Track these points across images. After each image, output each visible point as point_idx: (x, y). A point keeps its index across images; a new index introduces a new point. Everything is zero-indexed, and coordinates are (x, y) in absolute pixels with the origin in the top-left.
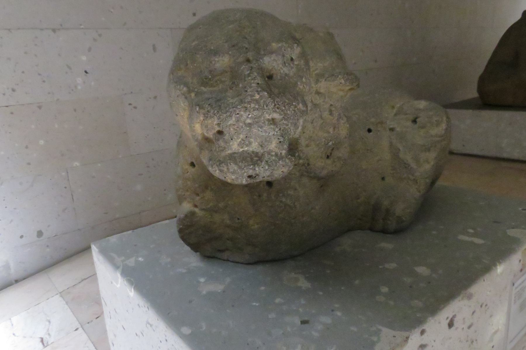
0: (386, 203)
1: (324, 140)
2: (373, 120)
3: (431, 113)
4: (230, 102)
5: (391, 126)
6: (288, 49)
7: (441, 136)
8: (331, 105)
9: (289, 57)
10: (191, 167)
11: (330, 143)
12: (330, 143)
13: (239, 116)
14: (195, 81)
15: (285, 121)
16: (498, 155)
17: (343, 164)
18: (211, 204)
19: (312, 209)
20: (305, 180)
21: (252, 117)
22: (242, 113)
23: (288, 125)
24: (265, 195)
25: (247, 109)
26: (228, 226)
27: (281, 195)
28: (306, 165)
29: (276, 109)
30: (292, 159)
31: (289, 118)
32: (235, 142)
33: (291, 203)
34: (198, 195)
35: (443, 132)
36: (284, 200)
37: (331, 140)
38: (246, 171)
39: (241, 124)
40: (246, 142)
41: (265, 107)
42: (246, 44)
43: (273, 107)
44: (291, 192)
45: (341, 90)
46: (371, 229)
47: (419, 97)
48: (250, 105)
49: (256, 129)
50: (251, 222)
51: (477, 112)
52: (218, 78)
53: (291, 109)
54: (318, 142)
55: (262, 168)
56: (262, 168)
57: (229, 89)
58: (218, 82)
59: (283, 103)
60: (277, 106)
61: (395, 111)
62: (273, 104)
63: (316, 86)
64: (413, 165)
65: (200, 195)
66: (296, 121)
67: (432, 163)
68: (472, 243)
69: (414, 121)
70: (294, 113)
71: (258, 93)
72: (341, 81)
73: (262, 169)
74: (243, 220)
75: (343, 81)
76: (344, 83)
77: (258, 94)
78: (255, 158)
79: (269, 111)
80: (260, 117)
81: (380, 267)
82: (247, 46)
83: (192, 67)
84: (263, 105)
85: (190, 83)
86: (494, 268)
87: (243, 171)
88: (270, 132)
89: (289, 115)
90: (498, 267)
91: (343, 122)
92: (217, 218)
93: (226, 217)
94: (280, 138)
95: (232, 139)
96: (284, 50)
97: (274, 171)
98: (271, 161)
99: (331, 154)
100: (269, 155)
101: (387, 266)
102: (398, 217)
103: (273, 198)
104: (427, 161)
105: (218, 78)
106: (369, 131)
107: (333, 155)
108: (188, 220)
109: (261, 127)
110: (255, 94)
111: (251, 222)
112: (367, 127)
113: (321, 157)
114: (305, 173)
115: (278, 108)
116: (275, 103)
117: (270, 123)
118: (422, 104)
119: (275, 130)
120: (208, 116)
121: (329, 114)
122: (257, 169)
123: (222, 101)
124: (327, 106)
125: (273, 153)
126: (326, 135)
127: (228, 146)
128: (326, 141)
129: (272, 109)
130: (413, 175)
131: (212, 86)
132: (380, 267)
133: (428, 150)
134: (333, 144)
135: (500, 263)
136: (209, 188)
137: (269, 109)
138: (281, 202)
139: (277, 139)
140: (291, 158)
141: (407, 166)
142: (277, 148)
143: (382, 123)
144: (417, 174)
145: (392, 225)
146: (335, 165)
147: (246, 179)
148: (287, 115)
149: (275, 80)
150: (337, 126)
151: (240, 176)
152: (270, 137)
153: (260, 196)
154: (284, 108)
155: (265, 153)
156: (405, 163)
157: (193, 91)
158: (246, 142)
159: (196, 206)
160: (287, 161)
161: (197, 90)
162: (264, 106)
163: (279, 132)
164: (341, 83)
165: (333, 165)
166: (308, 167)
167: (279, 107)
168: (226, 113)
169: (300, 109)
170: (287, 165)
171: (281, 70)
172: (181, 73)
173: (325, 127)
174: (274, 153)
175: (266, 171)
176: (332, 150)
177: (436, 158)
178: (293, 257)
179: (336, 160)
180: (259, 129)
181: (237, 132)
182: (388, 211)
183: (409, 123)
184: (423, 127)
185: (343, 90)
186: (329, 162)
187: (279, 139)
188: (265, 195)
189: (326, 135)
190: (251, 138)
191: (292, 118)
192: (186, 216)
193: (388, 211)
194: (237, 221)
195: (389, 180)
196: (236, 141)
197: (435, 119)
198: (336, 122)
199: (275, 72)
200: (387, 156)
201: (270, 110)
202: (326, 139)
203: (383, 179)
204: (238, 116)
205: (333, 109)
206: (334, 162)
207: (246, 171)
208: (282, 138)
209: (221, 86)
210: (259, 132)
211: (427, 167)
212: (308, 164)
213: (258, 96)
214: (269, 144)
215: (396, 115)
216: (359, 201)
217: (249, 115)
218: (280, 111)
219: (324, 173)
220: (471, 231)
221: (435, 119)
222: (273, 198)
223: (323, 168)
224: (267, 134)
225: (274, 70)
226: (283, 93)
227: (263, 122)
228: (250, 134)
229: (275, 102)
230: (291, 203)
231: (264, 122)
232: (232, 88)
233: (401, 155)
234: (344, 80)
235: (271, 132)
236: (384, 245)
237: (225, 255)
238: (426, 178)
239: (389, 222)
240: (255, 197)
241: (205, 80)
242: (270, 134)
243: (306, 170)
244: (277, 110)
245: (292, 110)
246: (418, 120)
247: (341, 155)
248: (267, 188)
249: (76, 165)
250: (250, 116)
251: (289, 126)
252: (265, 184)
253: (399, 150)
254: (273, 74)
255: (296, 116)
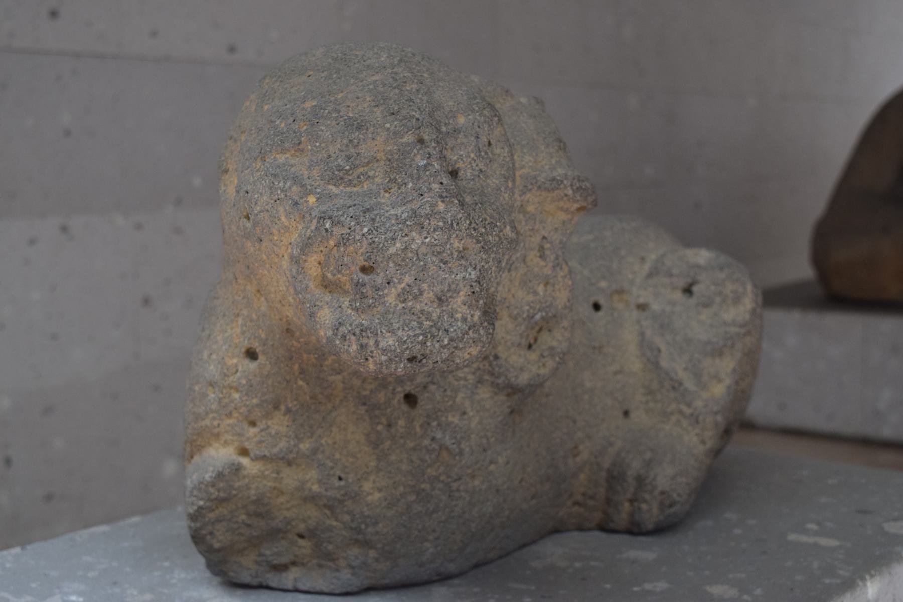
0: (635, 466)
1: (527, 308)
2: (603, 284)
3: (722, 276)
4: (390, 214)
5: (641, 300)
6: (485, 126)
7: (742, 326)
8: (544, 238)
9: (485, 140)
10: (247, 361)
11: (538, 316)
12: (538, 316)
13: (408, 240)
14: (315, 173)
15: (484, 254)
16: (870, 430)
17: (559, 363)
18: (283, 445)
19: (491, 462)
20: (484, 393)
21: (430, 242)
22: (414, 234)
23: (487, 263)
24: (401, 423)
25: (423, 228)
26: (311, 499)
27: (435, 424)
28: (491, 358)
29: (472, 230)
30: (489, 329)
31: (490, 248)
32: (393, 290)
33: (453, 444)
34: (253, 424)
35: (748, 316)
36: (439, 435)
37: (539, 310)
38: (410, 347)
39: (410, 255)
40: (413, 291)
41: (454, 225)
42: (416, 112)
43: (467, 226)
44: (454, 419)
45: (562, 209)
46: (604, 528)
47: (689, 243)
48: (430, 220)
49: (436, 266)
50: (367, 486)
51: (813, 318)
52: (361, 170)
53: (494, 233)
54: (515, 312)
55: (438, 341)
56: (438, 341)
57: (382, 191)
58: (362, 177)
59: (482, 221)
60: (473, 225)
61: (647, 267)
62: (468, 222)
63: (522, 198)
64: (689, 384)
65: (258, 424)
66: (501, 257)
67: (728, 381)
68: (816, 545)
69: (688, 291)
70: (499, 241)
71: (443, 199)
72: (566, 192)
73: (437, 345)
74: (350, 480)
75: (570, 192)
76: (571, 196)
77: (443, 201)
78: (425, 323)
79: (460, 233)
80: (446, 243)
81: (635, 589)
82: (417, 116)
83: (309, 147)
84: (452, 221)
85: (305, 177)
86: (860, 583)
87: (405, 347)
88: (459, 273)
89: (491, 243)
90: (869, 584)
91: (562, 274)
92: (290, 478)
93: (313, 474)
94: (474, 284)
95: (388, 283)
96: (477, 127)
97: (456, 351)
98: (455, 330)
99: (536, 340)
100: (452, 317)
101: (648, 586)
102: (663, 493)
103: (418, 430)
104: (717, 378)
105: (361, 170)
106: (597, 307)
107: (539, 342)
108: (221, 485)
109: (446, 263)
110: (437, 202)
111: (367, 486)
112: (593, 299)
113: (519, 345)
114: (487, 377)
115: (475, 229)
116: (469, 219)
117: (460, 256)
118: (703, 256)
119: (466, 270)
120: (350, 238)
121: (538, 254)
122: (429, 344)
123: (376, 212)
124: (536, 240)
125: (459, 315)
126: (531, 298)
127: (380, 296)
128: (531, 311)
129: (466, 230)
130: (689, 405)
131: (350, 183)
132: (635, 589)
133: (719, 353)
134: (543, 318)
135: (872, 576)
136: (283, 408)
137: (460, 231)
138: (433, 439)
139: (469, 287)
140: (488, 327)
141: (676, 386)
142: (467, 304)
143: (620, 292)
144: (699, 404)
145: (650, 513)
146: (544, 365)
147: (405, 364)
148: (488, 243)
149: (462, 179)
150: (551, 281)
151: (396, 357)
152: (457, 282)
153: (389, 426)
154: (483, 230)
155: (445, 313)
156: (672, 379)
157: (311, 192)
158: (413, 289)
159: (244, 452)
160: (482, 332)
161: (322, 191)
162: (452, 224)
163: (473, 273)
164: (566, 195)
165: (541, 364)
166: (495, 363)
167: (476, 227)
168: (385, 233)
169: (507, 235)
170: (480, 341)
171: (473, 162)
172: (283, 158)
173: (530, 281)
174: (460, 315)
175: (442, 350)
176: (540, 330)
177: (734, 370)
178: (444, 578)
179: (545, 354)
180: (442, 265)
181: (400, 270)
182: (640, 480)
183: (678, 296)
184: (706, 305)
185: (566, 211)
186: (533, 356)
187: (471, 286)
188: (401, 423)
189: (531, 298)
190: (423, 282)
191: (495, 249)
192: (220, 475)
193: (640, 480)
194: (337, 483)
195: (639, 417)
196: (396, 288)
197: (729, 288)
198: (549, 272)
199: (463, 165)
200: (636, 365)
201: (462, 231)
202: (531, 307)
203: (626, 414)
204: (406, 239)
205: (547, 246)
206: (542, 356)
207: (410, 346)
208: (478, 285)
209: (366, 186)
210: (440, 272)
211: (719, 390)
212: (496, 357)
213: (442, 206)
214: (454, 295)
215: (650, 275)
216: (578, 459)
217: (426, 238)
218: (478, 235)
219: (523, 379)
220: (812, 526)
221: (729, 288)
222: (418, 430)
223: (522, 369)
224: (453, 277)
225: (461, 162)
226: (481, 204)
227: (449, 252)
228: (424, 275)
229: (471, 218)
230: (453, 444)
231: (452, 254)
232: (390, 189)
233: (664, 363)
234: (573, 190)
235: (461, 272)
236: (632, 554)
237: (289, 578)
238: (716, 413)
239: (644, 506)
240: (380, 428)
241: (336, 172)
242: (458, 277)
243: (490, 369)
244: (473, 233)
245: (495, 235)
246: (695, 289)
247: (555, 344)
248: (405, 407)
249: (586, 186)
250: (427, 240)
251: (490, 264)
252: (402, 400)
253: (659, 351)
254: (458, 168)
255: (501, 247)
